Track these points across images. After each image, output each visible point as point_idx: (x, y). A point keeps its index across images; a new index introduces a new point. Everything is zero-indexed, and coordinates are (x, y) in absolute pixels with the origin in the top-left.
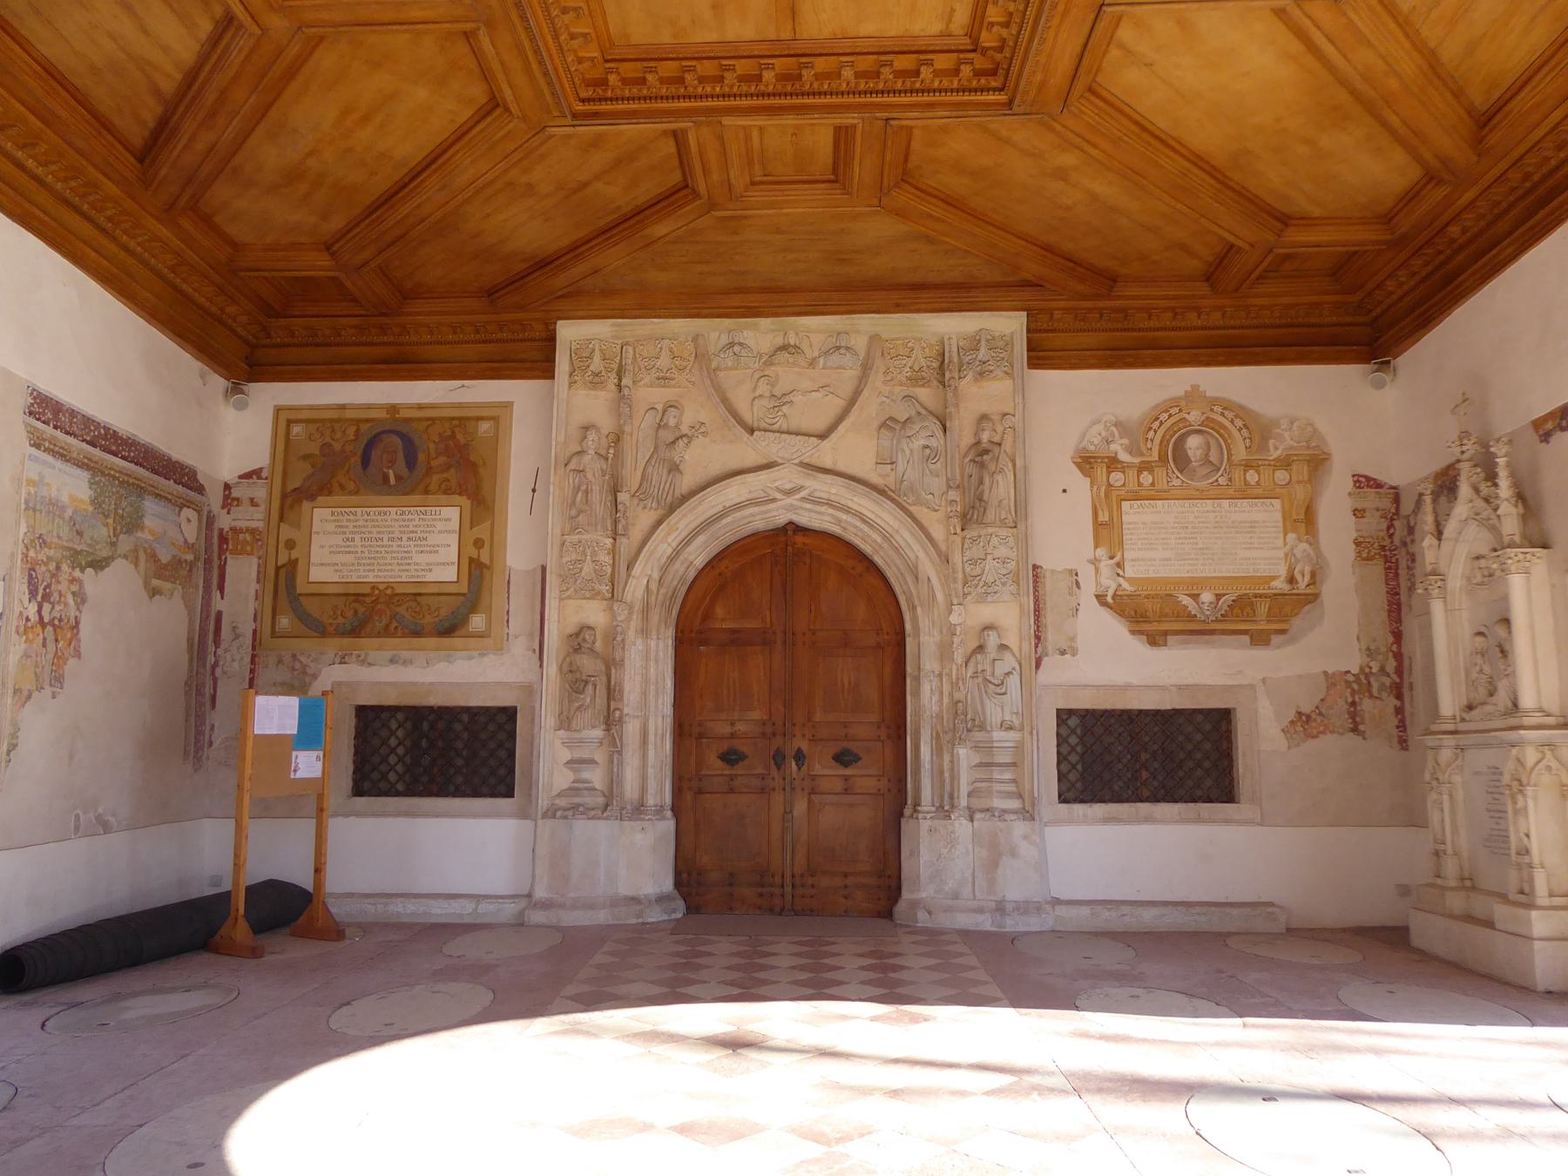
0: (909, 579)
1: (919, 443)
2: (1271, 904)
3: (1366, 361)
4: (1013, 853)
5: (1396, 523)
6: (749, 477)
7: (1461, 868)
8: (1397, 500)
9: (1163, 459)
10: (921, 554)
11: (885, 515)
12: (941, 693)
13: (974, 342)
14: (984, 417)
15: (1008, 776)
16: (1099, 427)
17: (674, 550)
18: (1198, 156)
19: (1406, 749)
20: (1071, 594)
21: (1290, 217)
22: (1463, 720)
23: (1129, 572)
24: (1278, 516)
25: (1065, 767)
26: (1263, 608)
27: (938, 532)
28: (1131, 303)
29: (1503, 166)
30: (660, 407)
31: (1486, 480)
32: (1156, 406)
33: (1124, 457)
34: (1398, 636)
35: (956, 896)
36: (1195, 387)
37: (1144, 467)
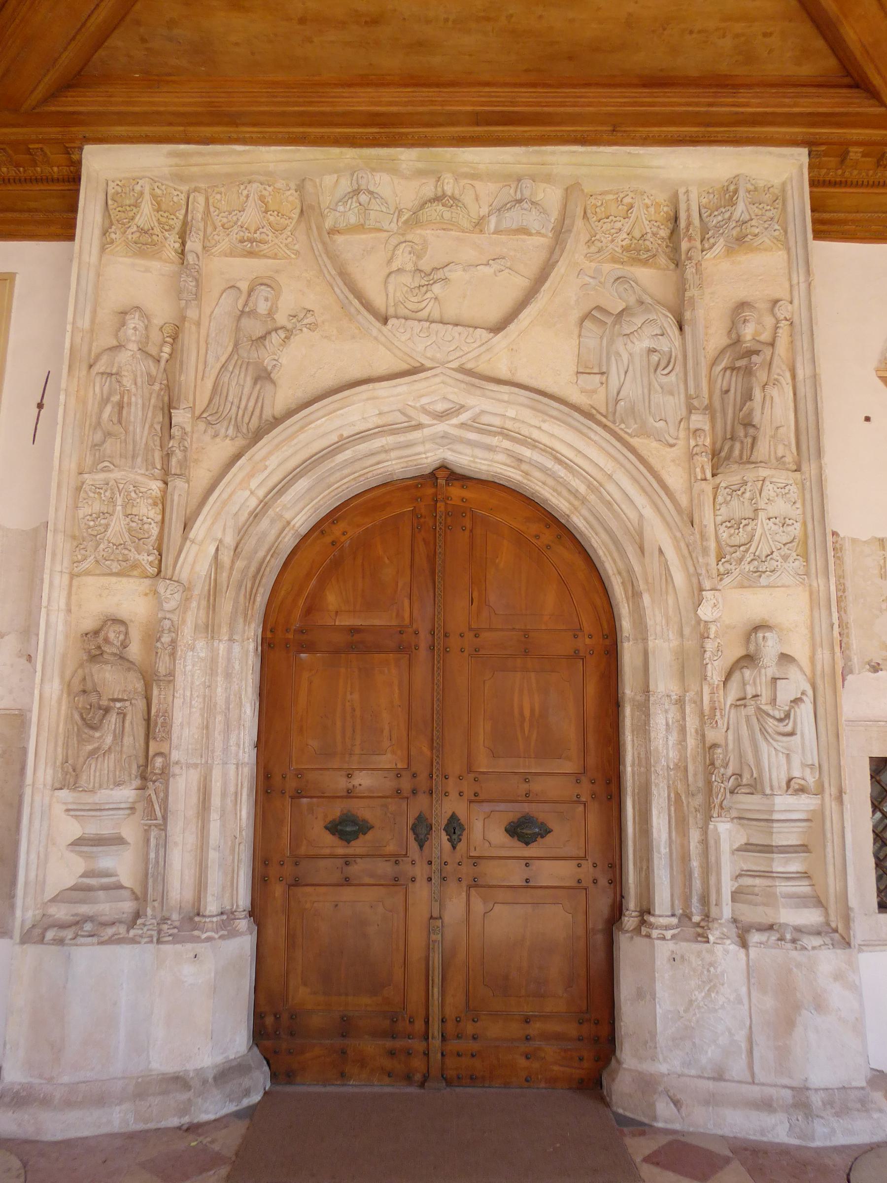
4: (819, 1005)
6: (382, 389)
12: (683, 730)
13: (728, 194)
17: (259, 502)
27: (675, 478)
30: (244, 286)
35: (719, 1076)
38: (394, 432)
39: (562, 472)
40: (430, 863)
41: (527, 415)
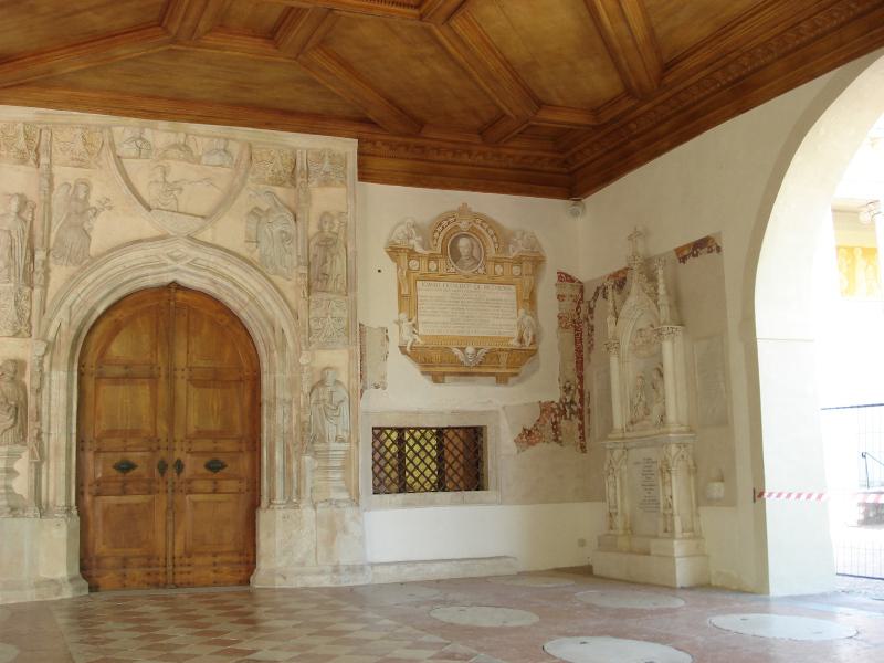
0: (269, 330)
1: (277, 229)
2: (505, 557)
3: (568, 199)
4: (345, 530)
5: (582, 305)
6: (147, 245)
7: (625, 522)
8: (582, 290)
9: (444, 252)
10: (277, 311)
11: (252, 282)
12: (291, 416)
13: (320, 157)
14: (326, 213)
15: (338, 476)
16: (403, 227)
17: (77, 295)
18: (508, 62)
19: (585, 452)
20: (383, 345)
21: (543, 103)
22: (628, 430)
23: (421, 331)
24: (514, 297)
25: (377, 469)
26: (504, 358)
27: (291, 296)
28: (427, 142)
29: (668, 94)
30: (72, 183)
31: (648, 281)
32: (439, 217)
33: (419, 249)
34: (581, 378)
35: (302, 564)
36: (465, 205)
37: (431, 257)
38: (152, 267)
39: (236, 290)
40: (167, 483)
41: (220, 261)
